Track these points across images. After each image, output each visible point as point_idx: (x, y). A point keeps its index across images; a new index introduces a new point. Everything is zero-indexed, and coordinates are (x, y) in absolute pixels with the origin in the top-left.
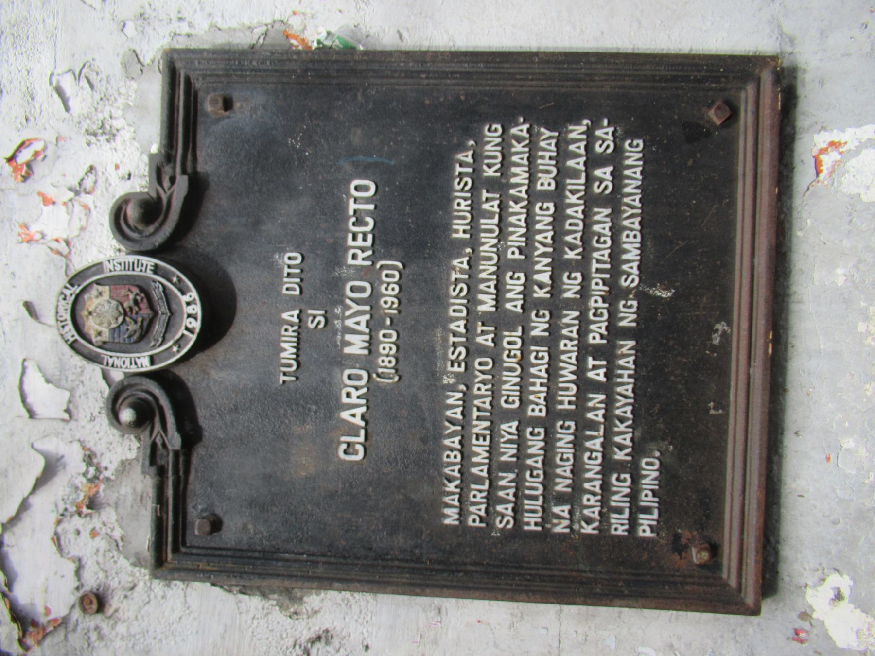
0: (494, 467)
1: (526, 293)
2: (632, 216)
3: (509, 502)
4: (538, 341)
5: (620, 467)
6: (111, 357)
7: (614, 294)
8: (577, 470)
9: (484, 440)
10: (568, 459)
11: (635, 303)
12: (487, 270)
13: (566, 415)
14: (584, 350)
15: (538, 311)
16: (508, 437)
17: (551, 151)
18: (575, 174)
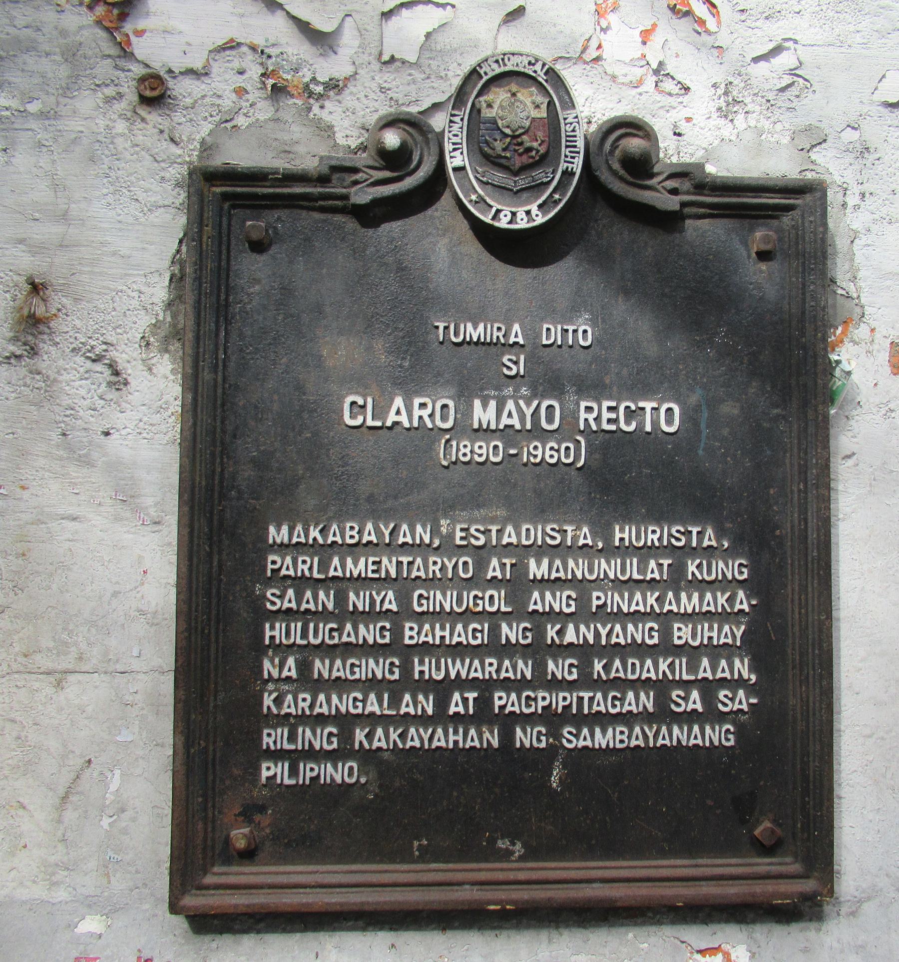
1: (552, 615)
3: (299, 603)
4: (495, 631)
5: (346, 736)
7: (552, 720)
8: (340, 685)
9: (373, 571)
13: (407, 669)
14: (486, 687)
16: (378, 600)
18: (693, 667)
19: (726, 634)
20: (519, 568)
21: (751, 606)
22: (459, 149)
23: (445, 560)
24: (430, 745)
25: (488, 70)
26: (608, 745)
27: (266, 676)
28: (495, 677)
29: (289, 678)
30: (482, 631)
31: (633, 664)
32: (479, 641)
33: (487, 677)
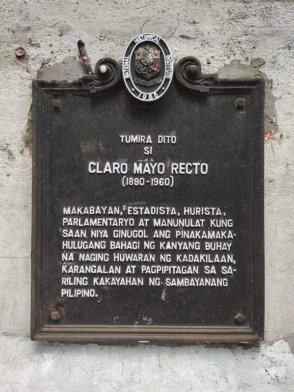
0: (88, 228)
1: (162, 239)
2: (195, 282)
4: (142, 245)
5: (91, 281)
7: (162, 276)
10: (93, 259)
14: (139, 264)
16: (101, 233)
20: (151, 223)
29: (71, 261)
31: (191, 257)
32: (136, 248)
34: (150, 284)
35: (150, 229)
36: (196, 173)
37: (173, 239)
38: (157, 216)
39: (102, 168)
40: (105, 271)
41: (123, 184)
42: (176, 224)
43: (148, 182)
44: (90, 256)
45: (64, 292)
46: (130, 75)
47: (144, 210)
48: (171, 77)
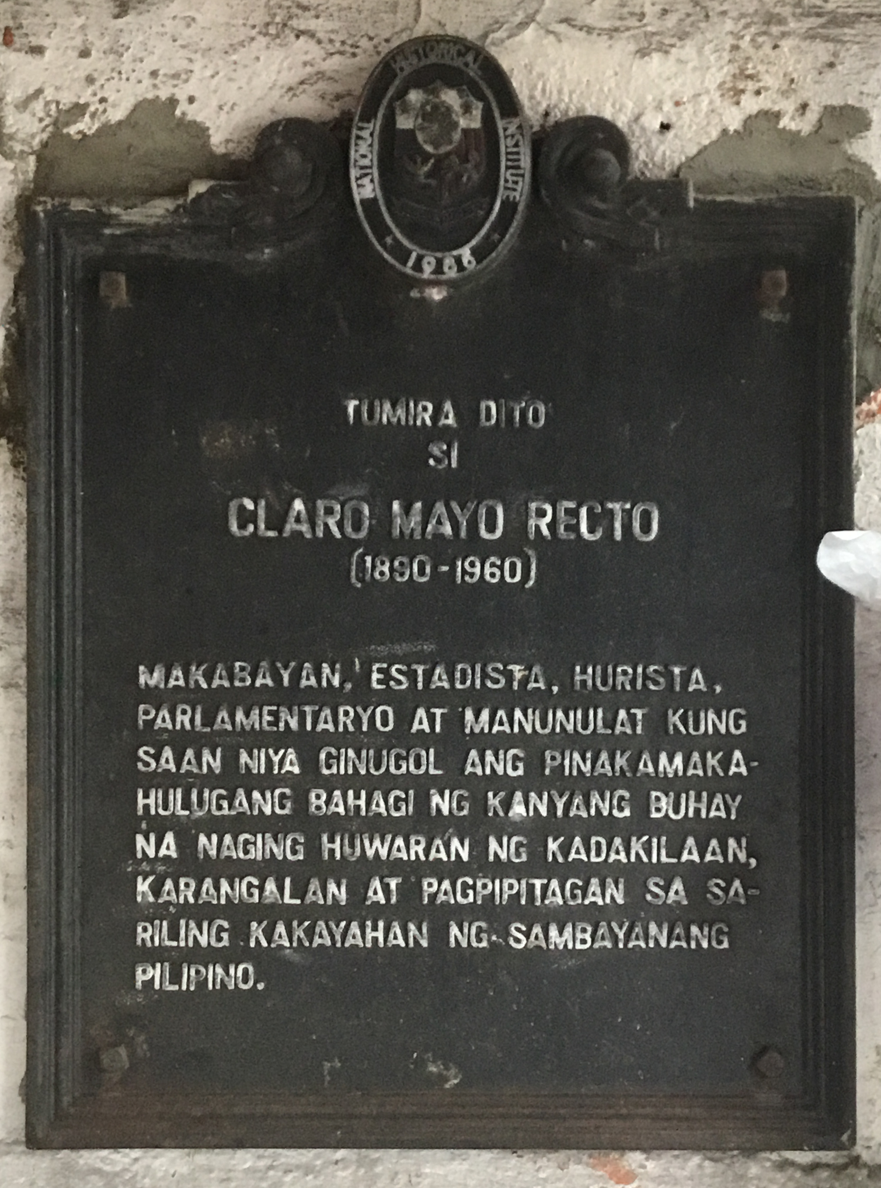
0: (233, 743)
1: (495, 781)
2: (615, 939)
3: (178, 765)
4: (423, 801)
5: (240, 932)
6: (372, 135)
7: (493, 914)
8: (234, 870)
9: (270, 723)
10: (246, 852)
11: (484, 944)
12: (527, 721)
13: (313, 848)
14: (412, 873)
15: (466, 799)
16: (276, 759)
17: (708, 810)
18: (675, 851)
19: (718, 805)
20: (454, 721)
21: (749, 769)
22: (366, 175)
23: (359, 709)
24: (343, 943)
25: (403, 64)
26: (566, 946)
27: (139, 855)
28: (423, 858)
29: (167, 858)
30: (406, 801)
31: (598, 844)
32: (403, 813)
33: (413, 858)
34: (453, 944)
35: (453, 744)
36: (618, 535)
37: (535, 780)
38: (478, 699)
39: (277, 520)
40: (292, 897)
41: (353, 580)
42: (544, 726)
43: (445, 568)
44: (235, 844)
45: (151, 974)
46: (378, 191)
47: (428, 675)
48: (521, 192)
